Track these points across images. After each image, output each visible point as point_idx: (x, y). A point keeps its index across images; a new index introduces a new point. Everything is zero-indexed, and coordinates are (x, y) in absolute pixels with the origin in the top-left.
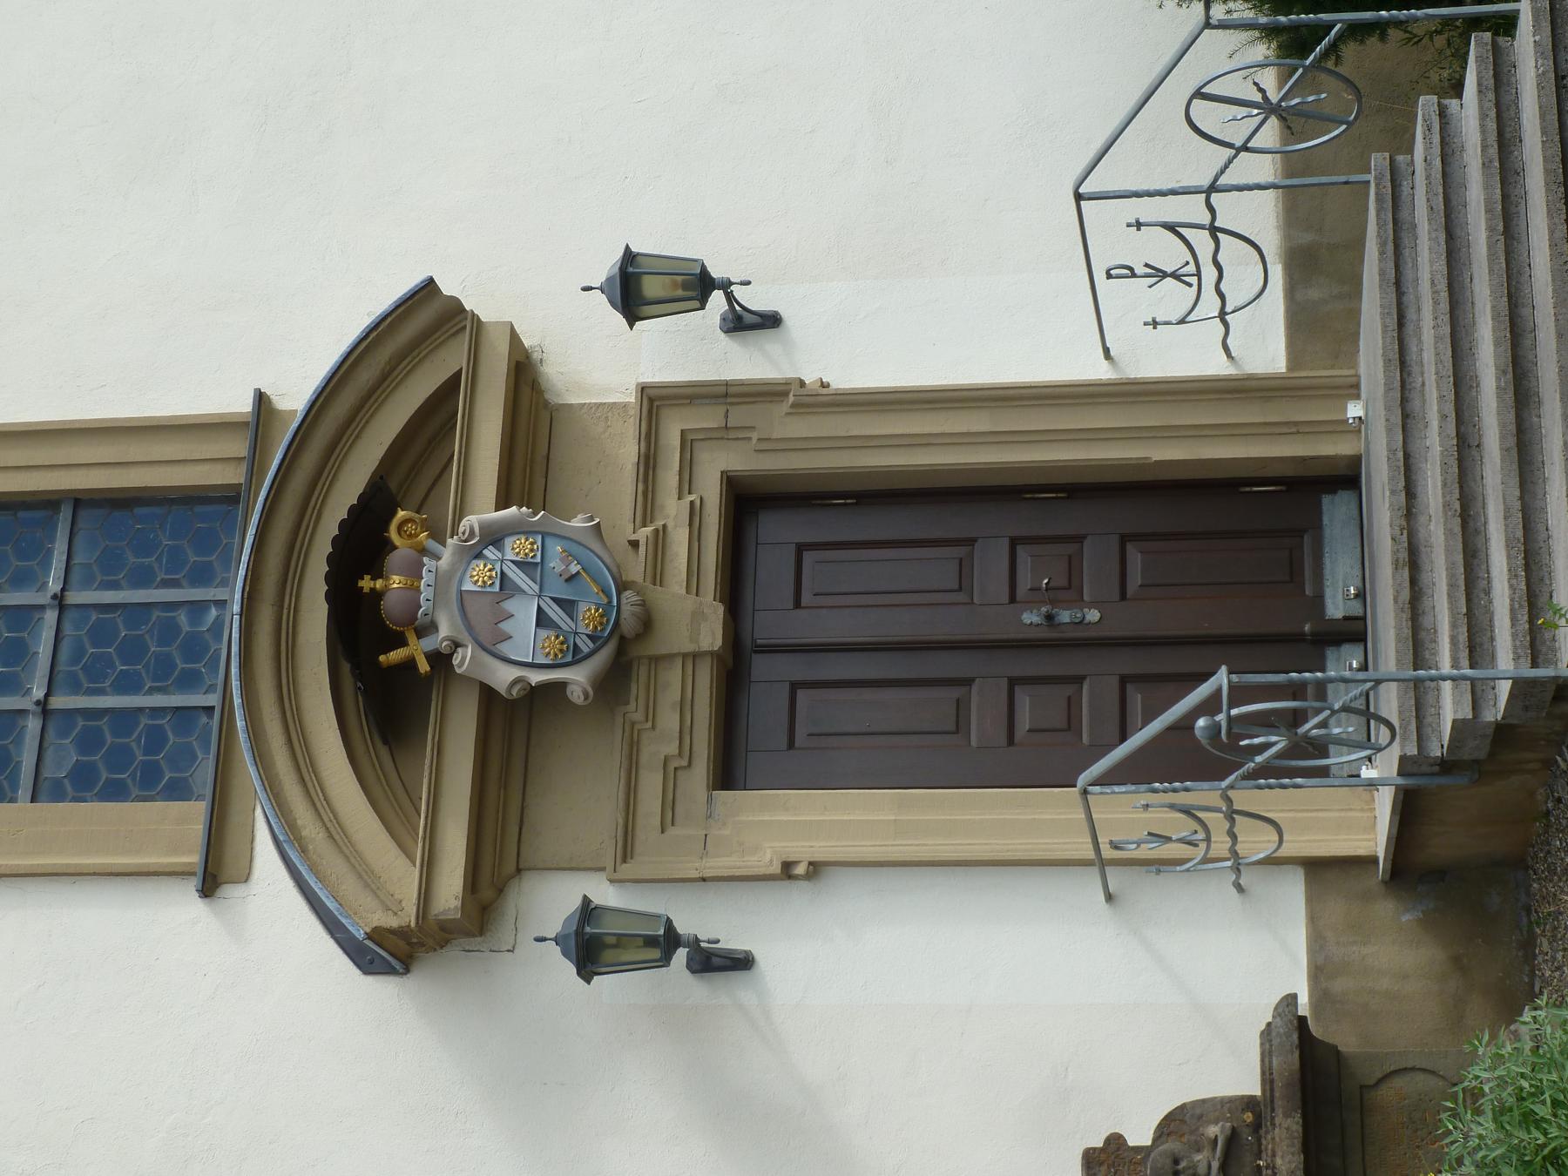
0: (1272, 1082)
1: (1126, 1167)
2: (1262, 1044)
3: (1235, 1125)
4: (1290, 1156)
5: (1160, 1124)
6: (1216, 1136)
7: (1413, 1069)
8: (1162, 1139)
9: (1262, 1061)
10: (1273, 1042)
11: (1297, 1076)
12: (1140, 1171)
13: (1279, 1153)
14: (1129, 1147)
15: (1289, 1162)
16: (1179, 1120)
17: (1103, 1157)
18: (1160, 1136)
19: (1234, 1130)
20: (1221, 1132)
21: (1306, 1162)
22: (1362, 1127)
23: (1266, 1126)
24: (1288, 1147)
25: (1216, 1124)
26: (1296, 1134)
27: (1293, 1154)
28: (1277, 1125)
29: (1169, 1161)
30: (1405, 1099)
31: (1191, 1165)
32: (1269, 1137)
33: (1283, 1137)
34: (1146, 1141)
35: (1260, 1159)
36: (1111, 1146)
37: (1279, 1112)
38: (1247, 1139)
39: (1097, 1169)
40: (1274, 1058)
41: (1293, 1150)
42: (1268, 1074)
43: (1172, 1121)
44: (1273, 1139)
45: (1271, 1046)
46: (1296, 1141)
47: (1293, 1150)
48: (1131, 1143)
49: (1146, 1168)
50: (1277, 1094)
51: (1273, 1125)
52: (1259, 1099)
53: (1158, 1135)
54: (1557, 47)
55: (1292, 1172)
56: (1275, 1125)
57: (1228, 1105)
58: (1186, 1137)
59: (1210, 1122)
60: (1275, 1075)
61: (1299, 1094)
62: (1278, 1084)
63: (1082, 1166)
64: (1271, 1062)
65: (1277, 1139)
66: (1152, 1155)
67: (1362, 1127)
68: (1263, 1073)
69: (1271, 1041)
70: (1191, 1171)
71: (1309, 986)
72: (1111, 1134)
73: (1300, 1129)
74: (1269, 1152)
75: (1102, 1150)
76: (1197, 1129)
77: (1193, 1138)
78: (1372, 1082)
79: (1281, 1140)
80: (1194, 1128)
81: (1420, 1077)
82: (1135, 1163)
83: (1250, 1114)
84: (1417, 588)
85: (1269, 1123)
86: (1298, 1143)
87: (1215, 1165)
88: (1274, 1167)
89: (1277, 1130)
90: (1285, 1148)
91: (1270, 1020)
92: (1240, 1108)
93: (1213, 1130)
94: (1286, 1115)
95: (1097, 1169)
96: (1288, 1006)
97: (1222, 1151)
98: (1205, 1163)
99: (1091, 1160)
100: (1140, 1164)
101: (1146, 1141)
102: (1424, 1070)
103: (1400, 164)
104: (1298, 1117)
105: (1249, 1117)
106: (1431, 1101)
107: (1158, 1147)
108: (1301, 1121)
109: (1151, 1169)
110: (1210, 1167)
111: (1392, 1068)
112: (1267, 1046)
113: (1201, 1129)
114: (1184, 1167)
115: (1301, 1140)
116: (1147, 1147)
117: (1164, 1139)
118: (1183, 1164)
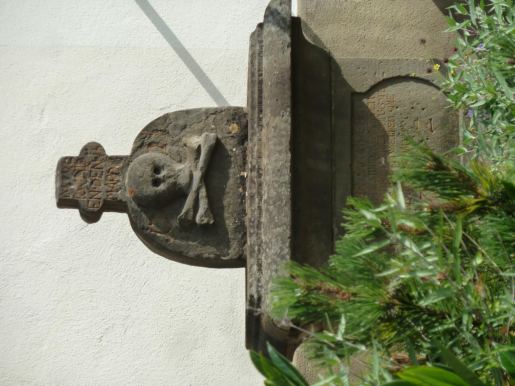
0: (261, 82)
1: (103, 178)
2: (252, 46)
3: (220, 137)
4: (278, 155)
5: (141, 134)
6: (199, 146)
7: (407, 78)
8: (142, 150)
9: (252, 63)
10: (264, 44)
11: (287, 75)
12: (118, 181)
13: (265, 153)
14: (107, 156)
15: (276, 161)
16: (161, 131)
17: (79, 166)
18: (140, 146)
19: (218, 140)
20: (205, 141)
21: (294, 161)
22: (352, 134)
23: (253, 127)
24: (275, 145)
25: (200, 135)
26: (284, 133)
27: (280, 152)
28: (265, 125)
29: (149, 170)
30: (397, 107)
31: (172, 173)
32: (255, 138)
33: (270, 136)
34: (126, 151)
35: (244, 170)
36: (89, 155)
37: (267, 111)
38: (232, 150)
39: (73, 178)
40: (264, 59)
41: (279, 148)
42: (257, 75)
43: (154, 131)
44: (260, 140)
45: (261, 47)
46: (284, 140)
47: (279, 148)
48: (110, 152)
49: (124, 177)
50: (265, 94)
51: (261, 126)
52: (246, 111)
53: (139, 144)
54: (140, 148)
55: (279, 170)
56: (262, 126)
57: (214, 116)
58: (168, 147)
59: (193, 133)
60: (265, 77)
61: (288, 93)
62: (267, 84)
63: (57, 176)
64: (260, 64)
65: (264, 140)
66: (132, 164)
67: (352, 134)
68: (252, 74)
69: (261, 42)
70: (172, 180)
71: (298, 5)
72: (89, 143)
73: (289, 128)
74: (255, 154)
75: (79, 159)
76: (180, 140)
77: (175, 148)
78: (364, 89)
79: (268, 139)
80: (176, 139)
81: (413, 85)
82: (112, 173)
83: (235, 125)
84: (472, 215)
85: (255, 125)
86: (286, 141)
87: (197, 175)
88: (259, 169)
89: (264, 131)
90: (272, 147)
91: (262, 21)
92: (225, 119)
93: (195, 141)
94: (275, 114)
95: (73, 178)
96: (281, 4)
97: (205, 161)
98: (187, 172)
99: (66, 170)
100: (117, 174)
101: (126, 151)
102: (417, 79)
103: (385, 372)
104: (287, 117)
105: (234, 128)
106: (423, 109)
107: (137, 156)
108: (290, 119)
109: (130, 177)
110: (191, 177)
111: (385, 76)
112: (258, 47)
113: (184, 139)
114: (164, 176)
115: (289, 139)
116: (126, 157)
117: (145, 148)
118: (163, 173)
